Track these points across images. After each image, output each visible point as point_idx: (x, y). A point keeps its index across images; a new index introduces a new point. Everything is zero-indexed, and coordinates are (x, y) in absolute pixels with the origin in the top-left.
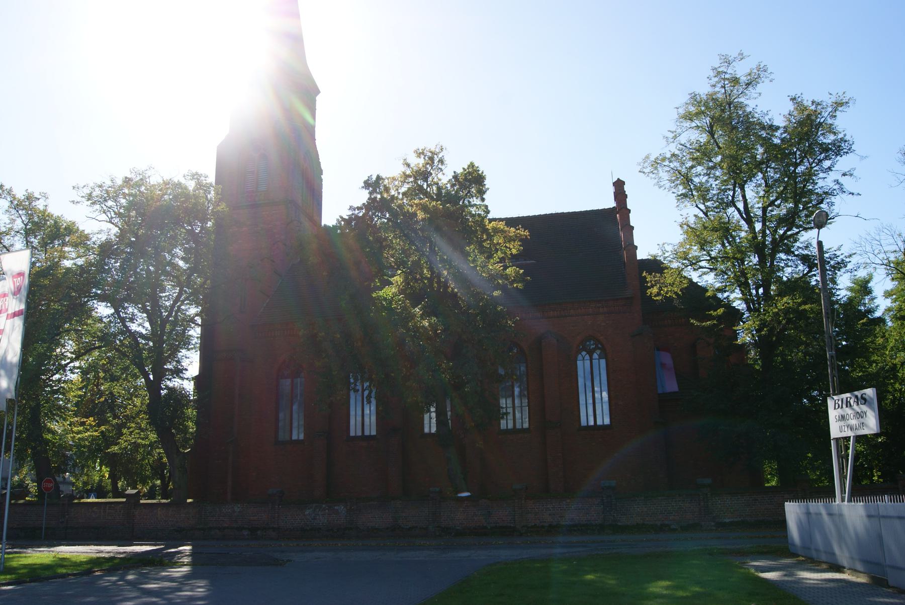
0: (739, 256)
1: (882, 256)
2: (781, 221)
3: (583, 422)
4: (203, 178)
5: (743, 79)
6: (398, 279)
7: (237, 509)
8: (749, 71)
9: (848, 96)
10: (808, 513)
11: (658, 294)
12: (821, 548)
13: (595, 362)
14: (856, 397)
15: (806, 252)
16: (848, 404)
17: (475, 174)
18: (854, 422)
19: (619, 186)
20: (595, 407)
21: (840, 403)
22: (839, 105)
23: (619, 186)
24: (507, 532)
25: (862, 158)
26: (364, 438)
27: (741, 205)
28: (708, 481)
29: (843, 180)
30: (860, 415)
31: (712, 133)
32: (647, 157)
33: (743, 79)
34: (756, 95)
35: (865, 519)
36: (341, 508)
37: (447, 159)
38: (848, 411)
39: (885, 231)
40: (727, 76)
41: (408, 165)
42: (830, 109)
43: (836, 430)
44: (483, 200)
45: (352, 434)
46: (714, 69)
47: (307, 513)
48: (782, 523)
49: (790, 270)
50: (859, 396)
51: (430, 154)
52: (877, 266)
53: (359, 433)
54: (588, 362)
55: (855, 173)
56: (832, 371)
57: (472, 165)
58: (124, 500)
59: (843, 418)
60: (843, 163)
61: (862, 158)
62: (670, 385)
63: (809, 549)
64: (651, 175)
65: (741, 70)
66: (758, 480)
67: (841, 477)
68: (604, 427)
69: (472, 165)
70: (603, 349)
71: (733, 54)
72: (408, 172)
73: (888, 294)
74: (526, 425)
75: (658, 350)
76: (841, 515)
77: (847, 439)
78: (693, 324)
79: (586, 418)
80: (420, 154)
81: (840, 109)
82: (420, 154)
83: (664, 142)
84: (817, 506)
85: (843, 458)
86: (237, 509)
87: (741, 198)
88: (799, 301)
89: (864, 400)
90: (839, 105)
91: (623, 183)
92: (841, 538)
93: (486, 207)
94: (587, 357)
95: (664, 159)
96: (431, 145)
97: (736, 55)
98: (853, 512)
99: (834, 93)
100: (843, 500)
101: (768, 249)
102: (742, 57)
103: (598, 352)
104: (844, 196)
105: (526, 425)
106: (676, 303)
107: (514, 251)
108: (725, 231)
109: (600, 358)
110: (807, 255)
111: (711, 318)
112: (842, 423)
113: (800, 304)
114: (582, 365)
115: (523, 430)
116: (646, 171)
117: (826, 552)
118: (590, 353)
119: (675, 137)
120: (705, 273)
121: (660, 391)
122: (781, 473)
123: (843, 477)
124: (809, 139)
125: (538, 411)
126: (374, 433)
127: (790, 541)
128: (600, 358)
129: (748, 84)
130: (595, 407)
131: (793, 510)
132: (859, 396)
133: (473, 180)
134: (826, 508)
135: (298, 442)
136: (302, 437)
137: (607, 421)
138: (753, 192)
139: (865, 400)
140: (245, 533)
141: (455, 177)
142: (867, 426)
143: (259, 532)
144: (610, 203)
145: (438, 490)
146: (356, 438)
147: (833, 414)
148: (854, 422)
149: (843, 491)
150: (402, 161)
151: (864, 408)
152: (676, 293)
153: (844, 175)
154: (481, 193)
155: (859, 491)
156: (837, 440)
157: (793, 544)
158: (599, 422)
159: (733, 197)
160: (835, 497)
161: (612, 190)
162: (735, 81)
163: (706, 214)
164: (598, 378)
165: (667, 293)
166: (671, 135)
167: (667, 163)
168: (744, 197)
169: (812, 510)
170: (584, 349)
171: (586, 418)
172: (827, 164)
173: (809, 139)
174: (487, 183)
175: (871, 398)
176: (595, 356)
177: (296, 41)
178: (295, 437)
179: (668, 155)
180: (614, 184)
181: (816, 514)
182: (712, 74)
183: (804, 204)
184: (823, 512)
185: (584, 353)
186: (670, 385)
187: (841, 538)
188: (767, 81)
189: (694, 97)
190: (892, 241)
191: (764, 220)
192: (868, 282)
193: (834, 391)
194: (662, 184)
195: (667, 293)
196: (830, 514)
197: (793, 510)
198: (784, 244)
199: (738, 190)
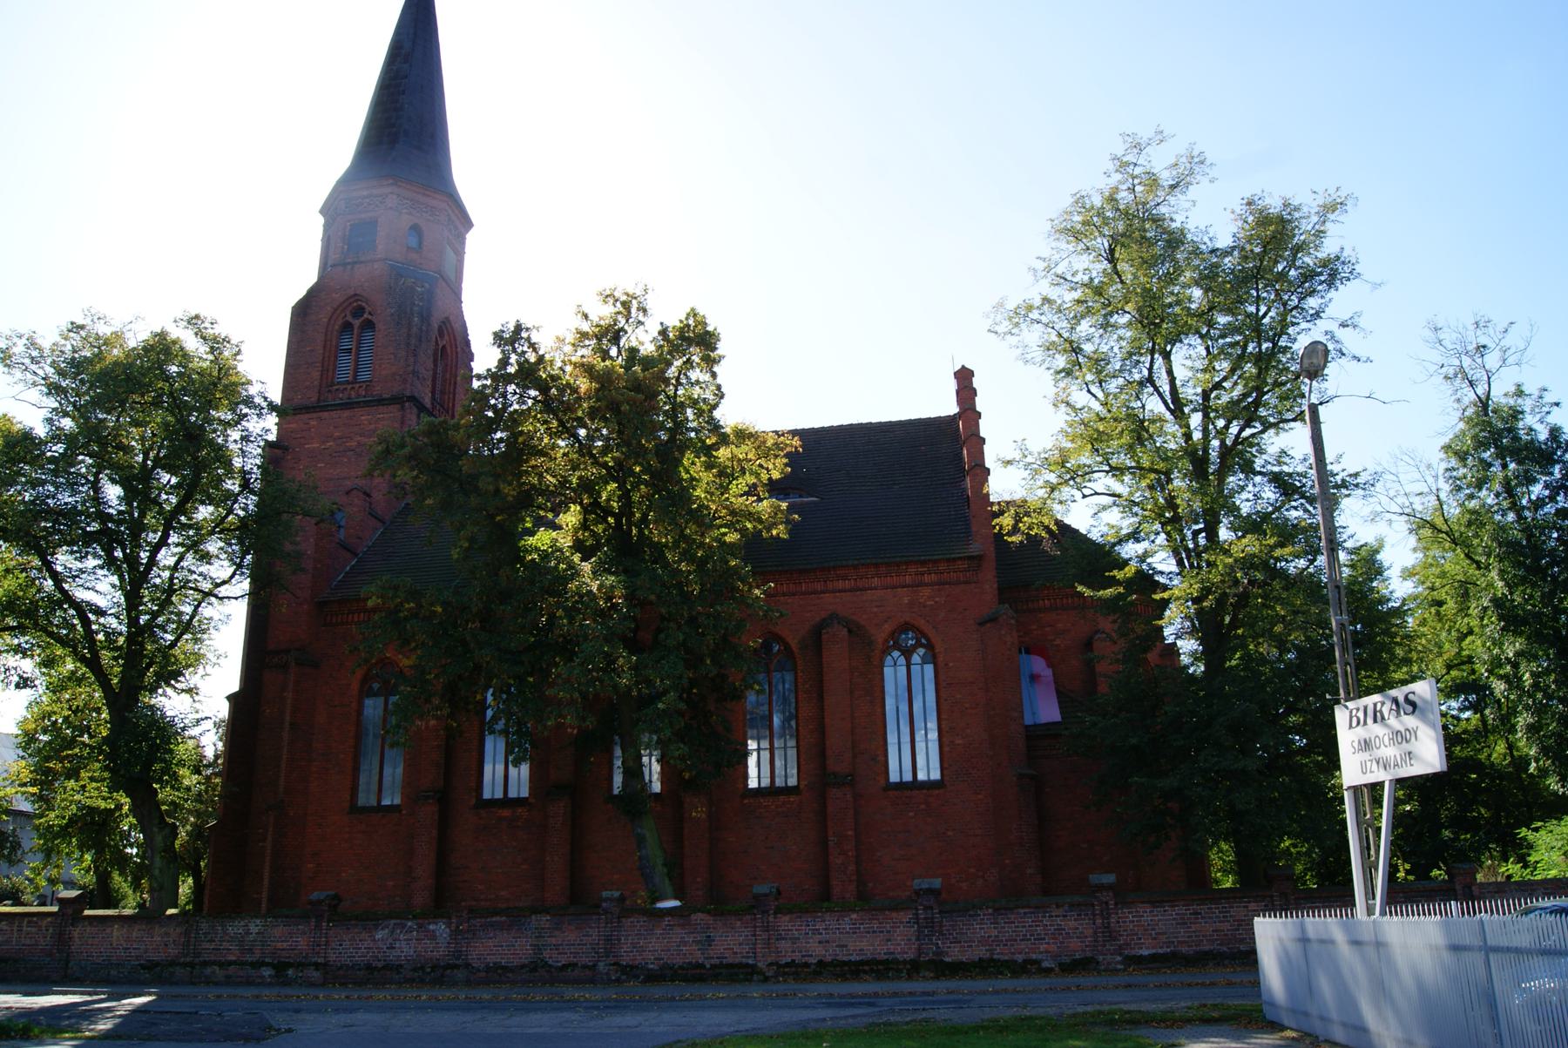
0: (1161, 466)
1: (1401, 500)
2: (1234, 411)
3: (894, 777)
4: (207, 325)
5: (1166, 178)
6: (571, 517)
7: (254, 929)
8: (1173, 161)
9: (1343, 193)
10: (1304, 940)
11: (1015, 530)
12: (1334, 1015)
13: (915, 669)
14: (1395, 701)
15: (1276, 469)
16: (1378, 717)
17: (699, 329)
18: (1390, 752)
19: (964, 378)
20: (915, 752)
21: (1361, 714)
22: (1331, 208)
23: (964, 378)
24: (736, 973)
25: (1377, 286)
26: (506, 802)
27: (1166, 388)
28: (1110, 878)
29: (1341, 334)
30: (1401, 737)
31: (1112, 259)
32: (1001, 305)
33: (1166, 178)
34: (1187, 205)
35: (1447, 956)
36: (441, 928)
37: (650, 304)
38: (1377, 730)
39: (1406, 458)
40: (1138, 171)
41: (586, 316)
42: (1315, 219)
43: (1353, 770)
44: (714, 375)
45: (487, 795)
46: (1115, 158)
47: (379, 936)
48: (1248, 957)
49: (1253, 496)
50: (1401, 699)
51: (624, 298)
52: (1394, 517)
53: (499, 795)
54: (904, 669)
55: (1362, 322)
56: (1342, 655)
57: (693, 313)
58: (55, 909)
59: (1366, 745)
60: (1340, 301)
61: (1377, 286)
62: (1045, 709)
63: (1306, 1014)
64: (1008, 337)
65: (1160, 162)
66: (1198, 883)
67: (1369, 858)
68: (929, 785)
69: (693, 313)
70: (930, 647)
71: (1145, 133)
72: (586, 327)
73: (1408, 574)
74: (793, 782)
75: (1028, 652)
76: (1380, 945)
77: (1376, 788)
78: (1081, 594)
79: (898, 768)
80: (608, 297)
81: (1331, 216)
82: (608, 297)
83: (1030, 277)
84: (1324, 924)
85: (1368, 828)
86: (254, 929)
87: (1163, 371)
88: (1272, 541)
89: (1413, 706)
90: (1331, 208)
91: (971, 373)
92: (1381, 990)
93: (719, 387)
94: (902, 660)
95: (1030, 308)
96: (626, 285)
97: (1151, 134)
98: (1416, 939)
99: (1320, 190)
100: (1370, 911)
101: (1214, 467)
102: (1161, 137)
103: (921, 651)
104: (1343, 361)
105: (793, 782)
106: (1047, 545)
107: (776, 475)
108: (1140, 430)
109: (924, 661)
110: (1280, 473)
111: (1113, 582)
112: (1365, 756)
113: (1273, 548)
114: (893, 674)
115: (787, 790)
116: (1001, 329)
117: (1344, 1025)
118: (907, 653)
119: (1048, 269)
120: (1104, 508)
121: (1028, 721)
122: (1243, 866)
123: (1369, 868)
124: (1277, 263)
125: (814, 756)
126: (525, 793)
127: (1265, 997)
128: (924, 661)
129: (1173, 187)
130: (915, 752)
131: (1271, 934)
132: (1401, 699)
133: (696, 340)
134: (1347, 929)
135: (391, 809)
136: (397, 801)
137: (936, 775)
138: (1187, 359)
139: (1413, 705)
140: (267, 972)
141: (663, 332)
142: (1419, 759)
143: (290, 972)
144: (949, 407)
145: (616, 894)
146: (493, 802)
147: (1346, 738)
148: (1390, 752)
149: (1370, 893)
150: (575, 309)
151: (1411, 721)
152: (1047, 528)
153: (1343, 325)
154: (710, 362)
155: (1399, 896)
156: (1356, 790)
157: (1272, 1004)
158: (921, 776)
159: (1150, 369)
160: (1354, 905)
161: (952, 385)
162: (1153, 182)
163: (1104, 404)
164: (920, 697)
165: (1030, 528)
166: (1041, 265)
167: (1035, 315)
168: (1170, 372)
169: (1311, 934)
170: (897, 646)
171: (898, 768)
172: (1313, 302)
173: (1277, 263)
174: (722, 348)
175: (1425, 701)
176: (916, 658)
177: (407, 112)
178: (386, 802)
179: (1037, 302)
180: (956, 374)
181: (1322, 941)
182: (1111, 166)
183: (1274, 377)
184: (1339, 935)
185: (896, 654)
186: (1045, 709)
187: (1381, 990)
188: (1205, 181)
189: (1080, 200)
190: (1418, 476)
191: (1205, 410)
192: (1377, 552)
193: (1347, 693)
194: (1029, 357)
195: (1030, 528)
196: (1356, 943)
197: (1271, 934)
198: (1238, 457)
199: (1159, 361)
